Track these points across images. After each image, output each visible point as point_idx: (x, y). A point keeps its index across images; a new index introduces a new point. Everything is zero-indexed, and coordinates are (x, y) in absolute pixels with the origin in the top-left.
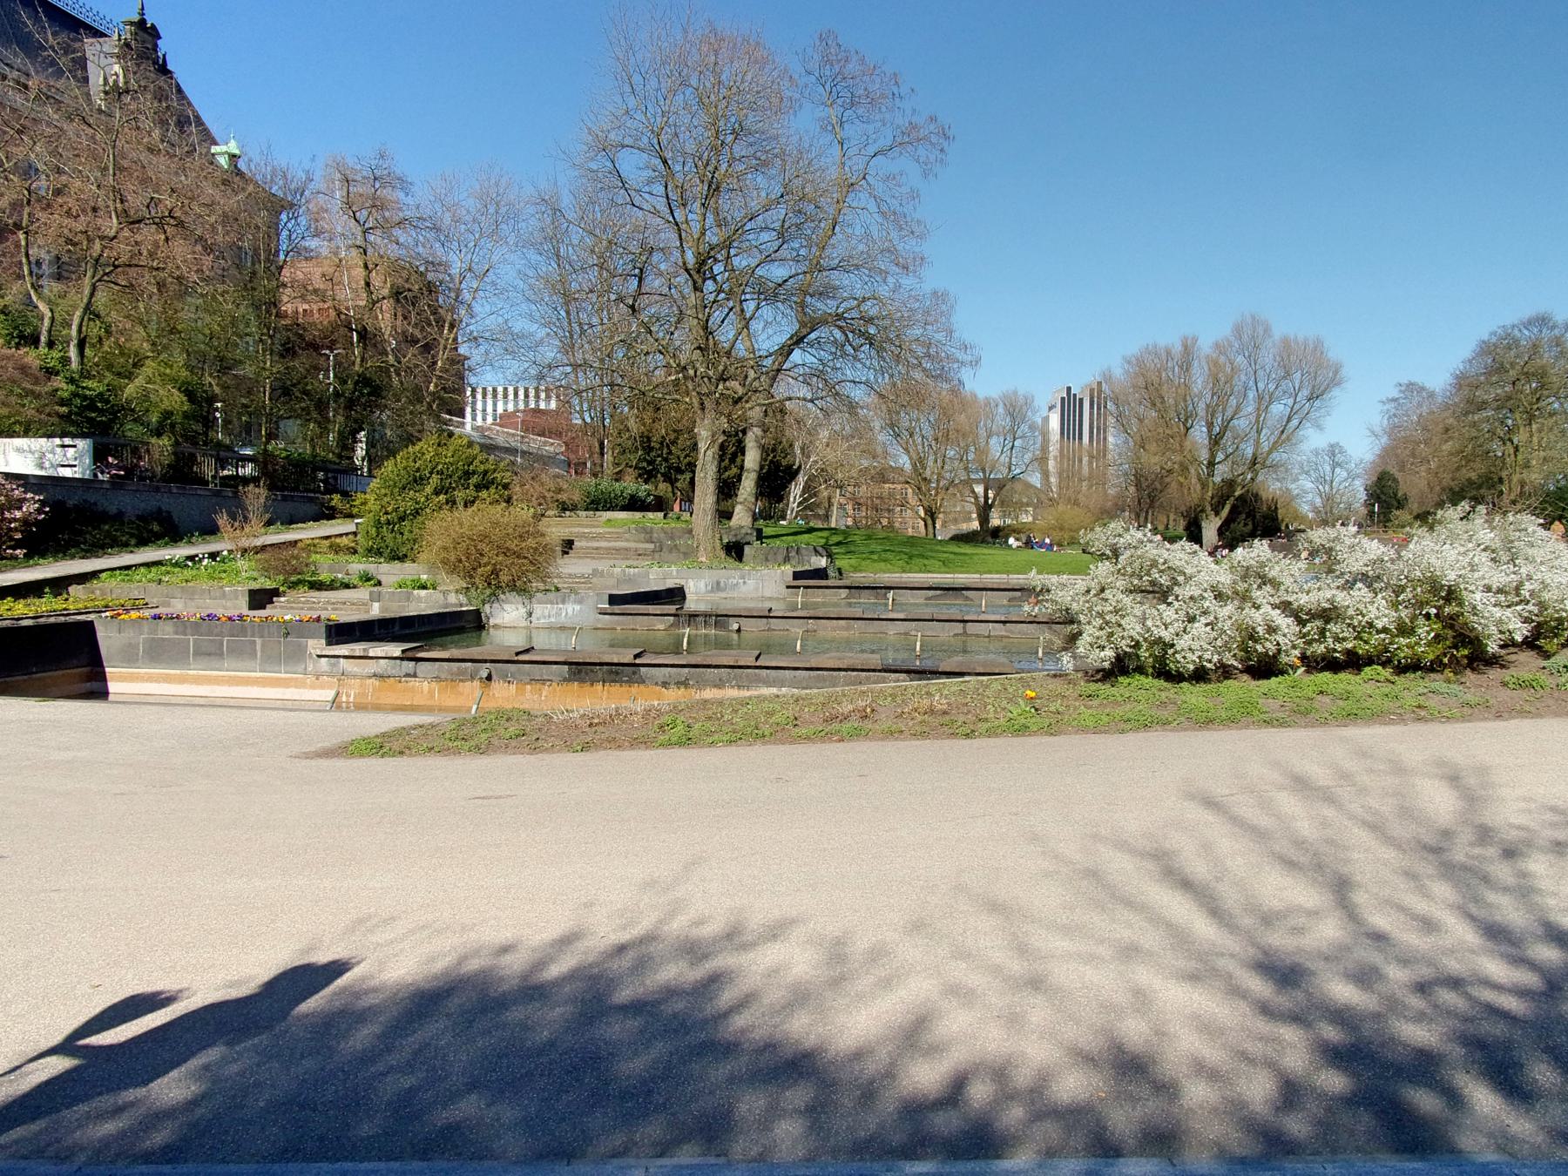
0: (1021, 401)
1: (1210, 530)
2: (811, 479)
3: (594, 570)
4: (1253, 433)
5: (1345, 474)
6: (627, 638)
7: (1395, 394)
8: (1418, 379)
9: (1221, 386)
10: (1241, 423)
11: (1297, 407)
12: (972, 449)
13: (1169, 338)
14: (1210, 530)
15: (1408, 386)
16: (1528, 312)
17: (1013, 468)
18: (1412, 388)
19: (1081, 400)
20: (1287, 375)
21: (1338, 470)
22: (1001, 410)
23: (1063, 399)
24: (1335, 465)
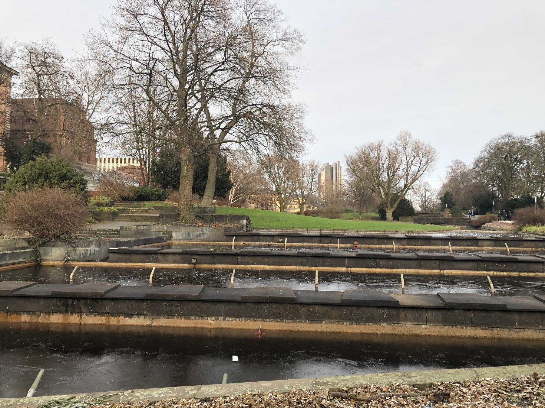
0: (316, 164)
1: (389, 214)
2: (237, 190)
3: (121, 227)
4: (406, 176)
5: (430, 194)
6: (348, 170)
7: (451, 164)
8: (460, 159)
9: (393, 158)
10: (401, 172)
11: (421, 167)
12: (297, 182)
13: (374, 140)
14: (389, 214)
15: (456, 161)
16: (504, 133)
17: (312, 189)
18: (458, 162)
19: (332, 168)
20: (418, 154)
21: (427, 192)
22: (308, 168)
23: (326, 167)
24: (426, 191)
